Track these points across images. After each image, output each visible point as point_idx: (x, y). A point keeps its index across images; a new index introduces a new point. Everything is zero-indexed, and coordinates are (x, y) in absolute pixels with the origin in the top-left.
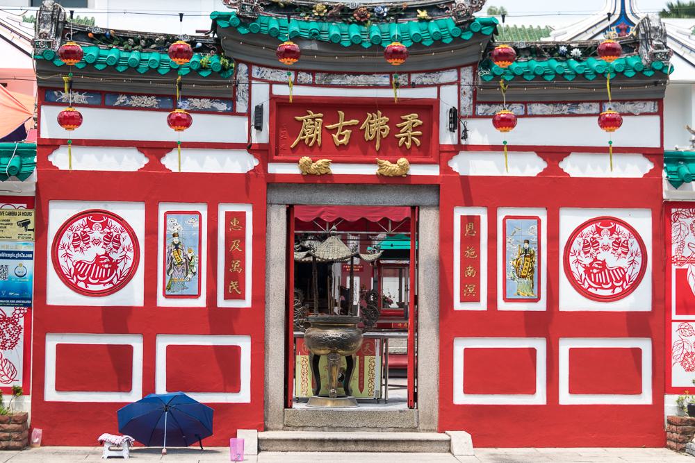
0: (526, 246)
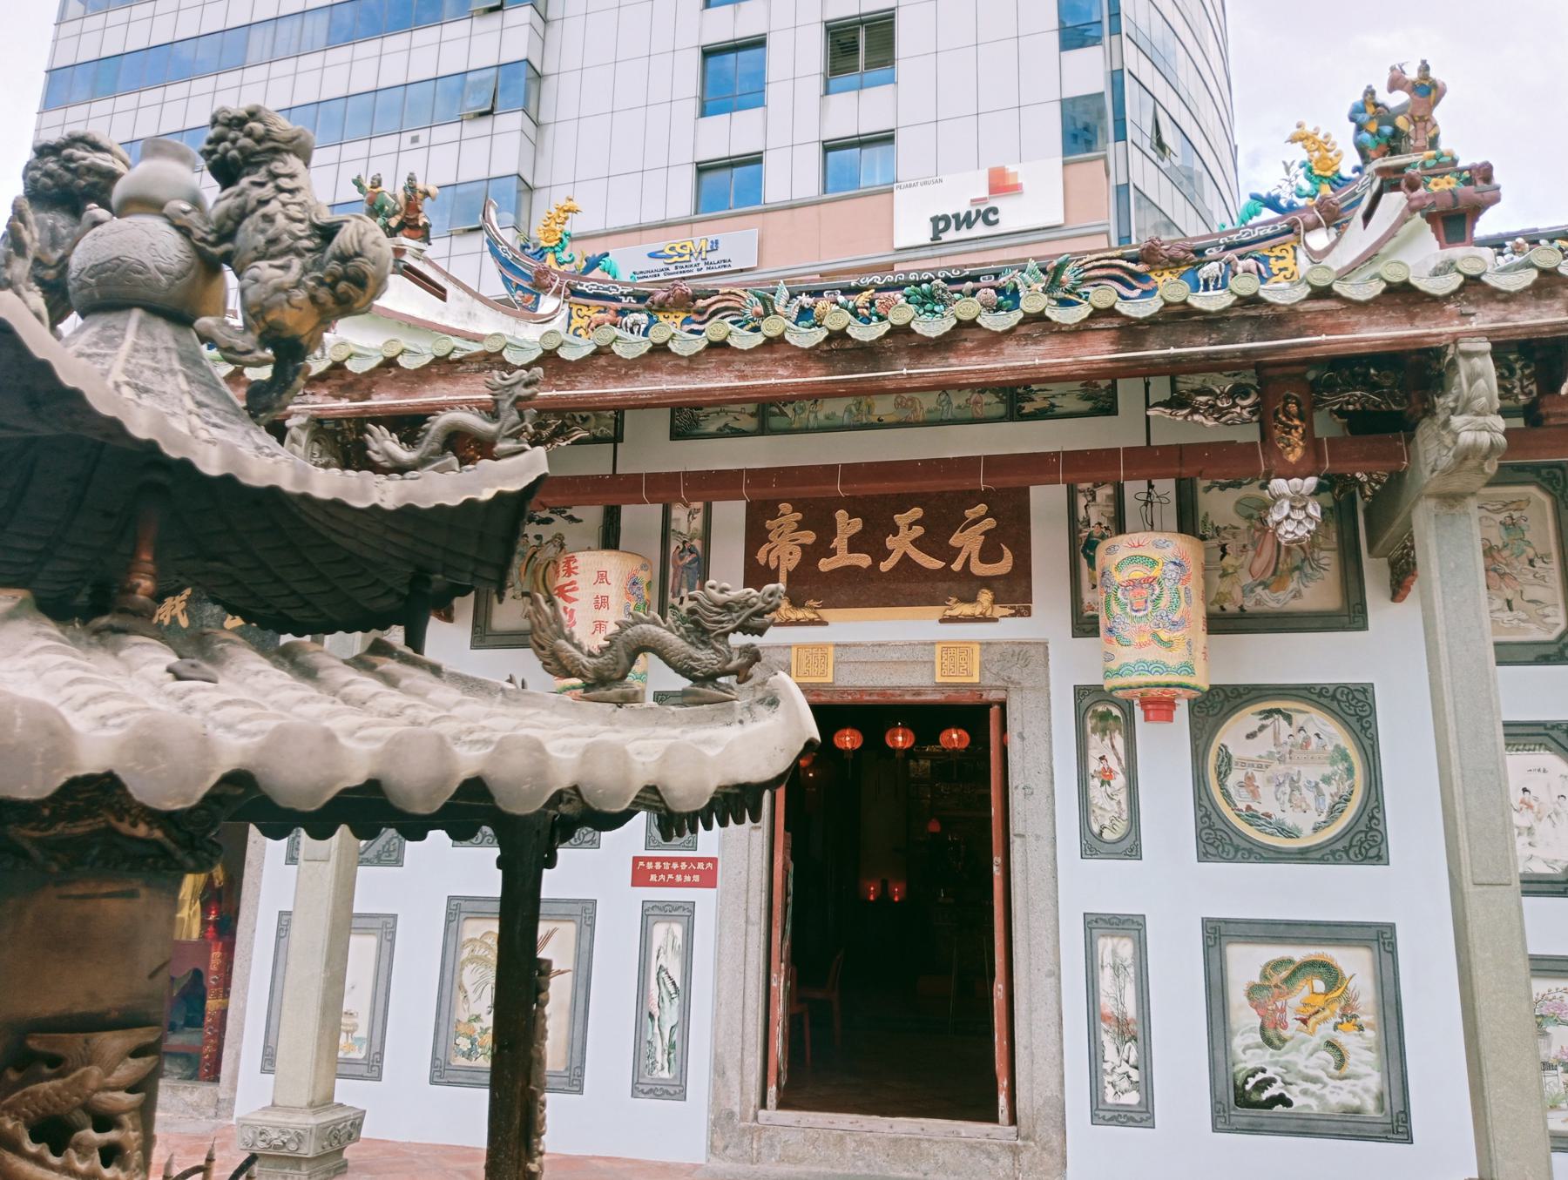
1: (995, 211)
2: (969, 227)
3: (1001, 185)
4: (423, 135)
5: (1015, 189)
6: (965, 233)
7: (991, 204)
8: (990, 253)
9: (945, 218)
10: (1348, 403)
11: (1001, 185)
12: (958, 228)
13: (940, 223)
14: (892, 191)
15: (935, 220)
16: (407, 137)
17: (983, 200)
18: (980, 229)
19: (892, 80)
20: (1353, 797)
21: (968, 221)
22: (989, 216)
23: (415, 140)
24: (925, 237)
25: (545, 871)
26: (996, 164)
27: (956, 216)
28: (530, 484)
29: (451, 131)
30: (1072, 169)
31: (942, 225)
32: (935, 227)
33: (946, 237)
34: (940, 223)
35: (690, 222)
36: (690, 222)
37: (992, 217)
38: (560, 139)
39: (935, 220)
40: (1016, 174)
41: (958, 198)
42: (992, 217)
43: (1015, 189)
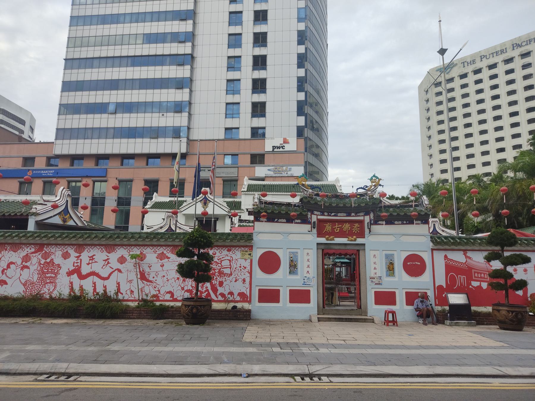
0: (391, 261)
1: (284, 146)
2: (279, 149)
3: (286, 141)
4: (165, 114)
5: (288, 143)
6: (278, 150)
7: (284, 145)
8: (200, 381)
9: (275, 146)
10: (317, 195)
11: (286, 141)
12: (277, 149)
13: (274, 147)
14: (265, 139)
15: (273, 147)
16: (161, 114)
17: (282, 144)
18: (281, 150)
19: (267, 24)
20: (226, 201)
21: (279, 148)
22: (283, 147)
23: (163, 115)
24: (271, 150)
25: (253, 220)
26: (285, 137)
27: (277, 146)
28: (512, 331)
29: (172, 114)
30: (299, 140)
31: (274, 148)
32: (273, 148)
33: (275, 150)
34: (274, 147)
35: (224, 140)
36: (224, 140)
37: (284, 148)
38: (195, 118)
39: (273, 147)
40: (288, 140)
41: (278, 142)
42: (284, 148)
43: (288, 143)
